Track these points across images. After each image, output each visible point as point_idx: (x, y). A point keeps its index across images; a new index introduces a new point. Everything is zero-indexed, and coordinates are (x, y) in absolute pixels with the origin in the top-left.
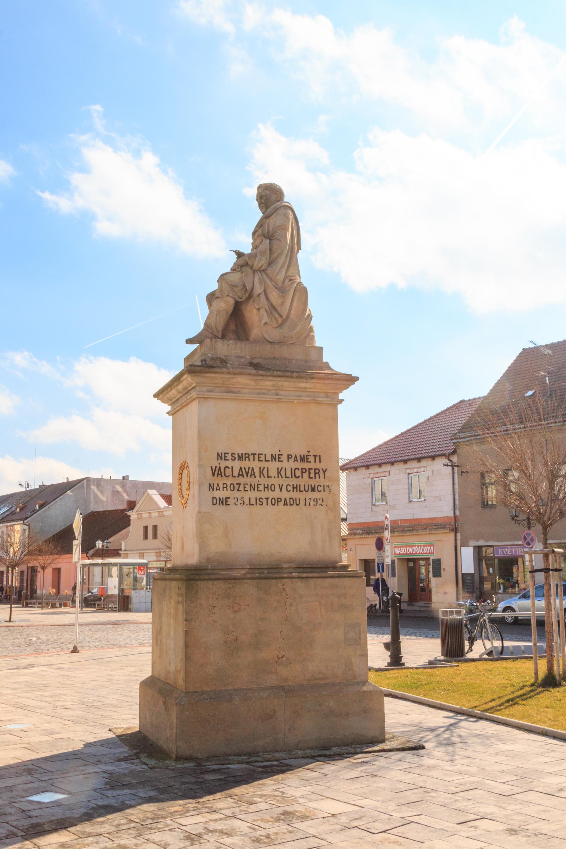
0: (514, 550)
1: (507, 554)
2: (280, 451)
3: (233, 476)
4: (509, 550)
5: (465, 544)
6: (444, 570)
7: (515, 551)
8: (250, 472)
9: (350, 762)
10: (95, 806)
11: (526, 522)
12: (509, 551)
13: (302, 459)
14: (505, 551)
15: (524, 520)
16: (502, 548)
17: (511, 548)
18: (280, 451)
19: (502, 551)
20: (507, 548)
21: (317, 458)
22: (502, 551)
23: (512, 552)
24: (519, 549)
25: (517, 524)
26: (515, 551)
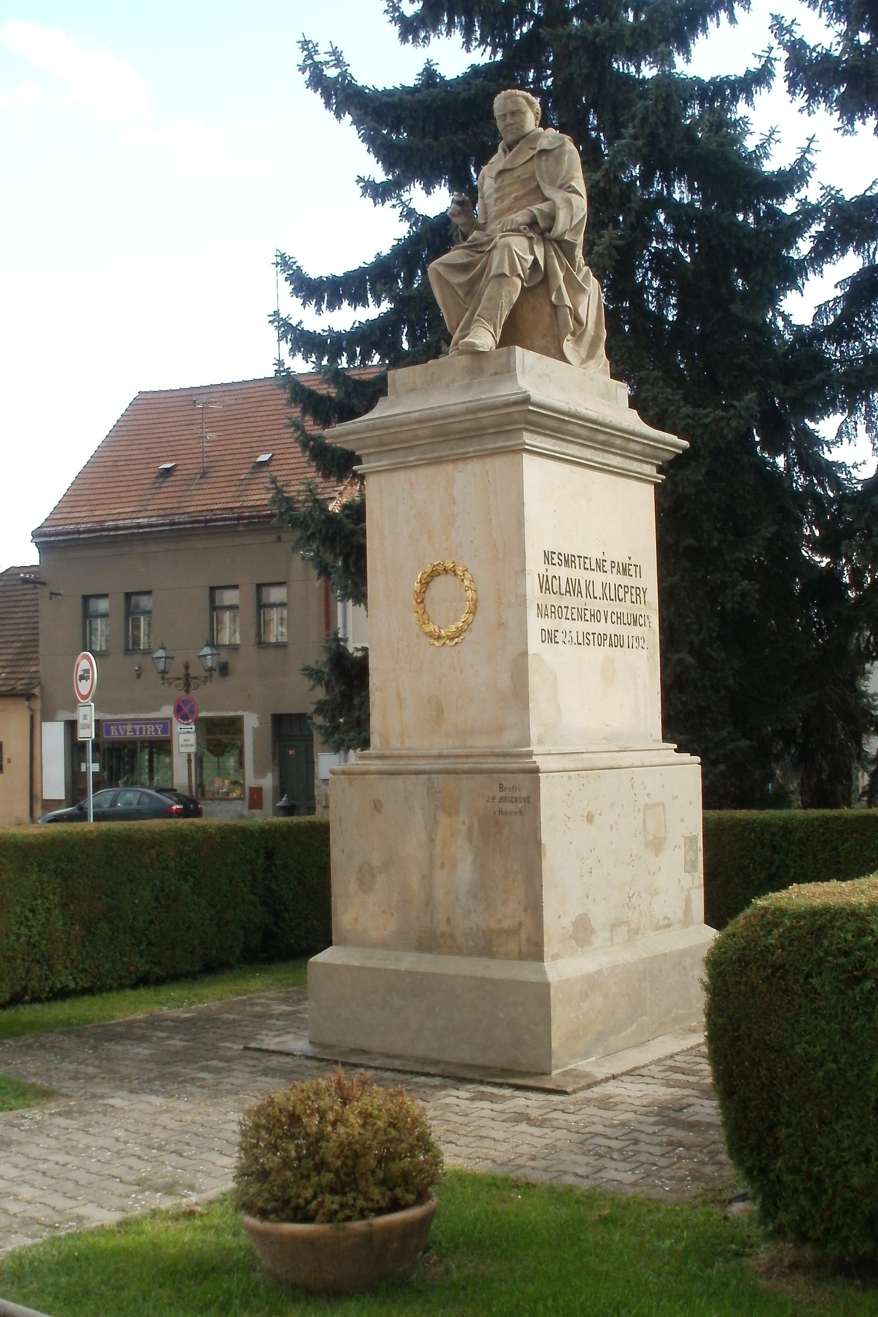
0: (137, 727)
1: (125, 734)
2: (630, 558)
3: (561, 594)
4: (129, 727)
5: (48, 716)
6: (9, 761)
7: (141, 731)
8: (573, 589)
9: (150, 1103)
10: (513, 1115)
11: (181, 682)
12: (129, 730)
13: (625, 570)
14: (123, 729)
15: (179, 679)
16: (117, 725)
17: (133, 724)
18: (630, 558)
19: (118, 730)
20: (126, 724)
21: (638, 568)
22: (118, 730)
23: (134, 730)
24: (148, 726)
25: (166, 685)
26: (141, 731)
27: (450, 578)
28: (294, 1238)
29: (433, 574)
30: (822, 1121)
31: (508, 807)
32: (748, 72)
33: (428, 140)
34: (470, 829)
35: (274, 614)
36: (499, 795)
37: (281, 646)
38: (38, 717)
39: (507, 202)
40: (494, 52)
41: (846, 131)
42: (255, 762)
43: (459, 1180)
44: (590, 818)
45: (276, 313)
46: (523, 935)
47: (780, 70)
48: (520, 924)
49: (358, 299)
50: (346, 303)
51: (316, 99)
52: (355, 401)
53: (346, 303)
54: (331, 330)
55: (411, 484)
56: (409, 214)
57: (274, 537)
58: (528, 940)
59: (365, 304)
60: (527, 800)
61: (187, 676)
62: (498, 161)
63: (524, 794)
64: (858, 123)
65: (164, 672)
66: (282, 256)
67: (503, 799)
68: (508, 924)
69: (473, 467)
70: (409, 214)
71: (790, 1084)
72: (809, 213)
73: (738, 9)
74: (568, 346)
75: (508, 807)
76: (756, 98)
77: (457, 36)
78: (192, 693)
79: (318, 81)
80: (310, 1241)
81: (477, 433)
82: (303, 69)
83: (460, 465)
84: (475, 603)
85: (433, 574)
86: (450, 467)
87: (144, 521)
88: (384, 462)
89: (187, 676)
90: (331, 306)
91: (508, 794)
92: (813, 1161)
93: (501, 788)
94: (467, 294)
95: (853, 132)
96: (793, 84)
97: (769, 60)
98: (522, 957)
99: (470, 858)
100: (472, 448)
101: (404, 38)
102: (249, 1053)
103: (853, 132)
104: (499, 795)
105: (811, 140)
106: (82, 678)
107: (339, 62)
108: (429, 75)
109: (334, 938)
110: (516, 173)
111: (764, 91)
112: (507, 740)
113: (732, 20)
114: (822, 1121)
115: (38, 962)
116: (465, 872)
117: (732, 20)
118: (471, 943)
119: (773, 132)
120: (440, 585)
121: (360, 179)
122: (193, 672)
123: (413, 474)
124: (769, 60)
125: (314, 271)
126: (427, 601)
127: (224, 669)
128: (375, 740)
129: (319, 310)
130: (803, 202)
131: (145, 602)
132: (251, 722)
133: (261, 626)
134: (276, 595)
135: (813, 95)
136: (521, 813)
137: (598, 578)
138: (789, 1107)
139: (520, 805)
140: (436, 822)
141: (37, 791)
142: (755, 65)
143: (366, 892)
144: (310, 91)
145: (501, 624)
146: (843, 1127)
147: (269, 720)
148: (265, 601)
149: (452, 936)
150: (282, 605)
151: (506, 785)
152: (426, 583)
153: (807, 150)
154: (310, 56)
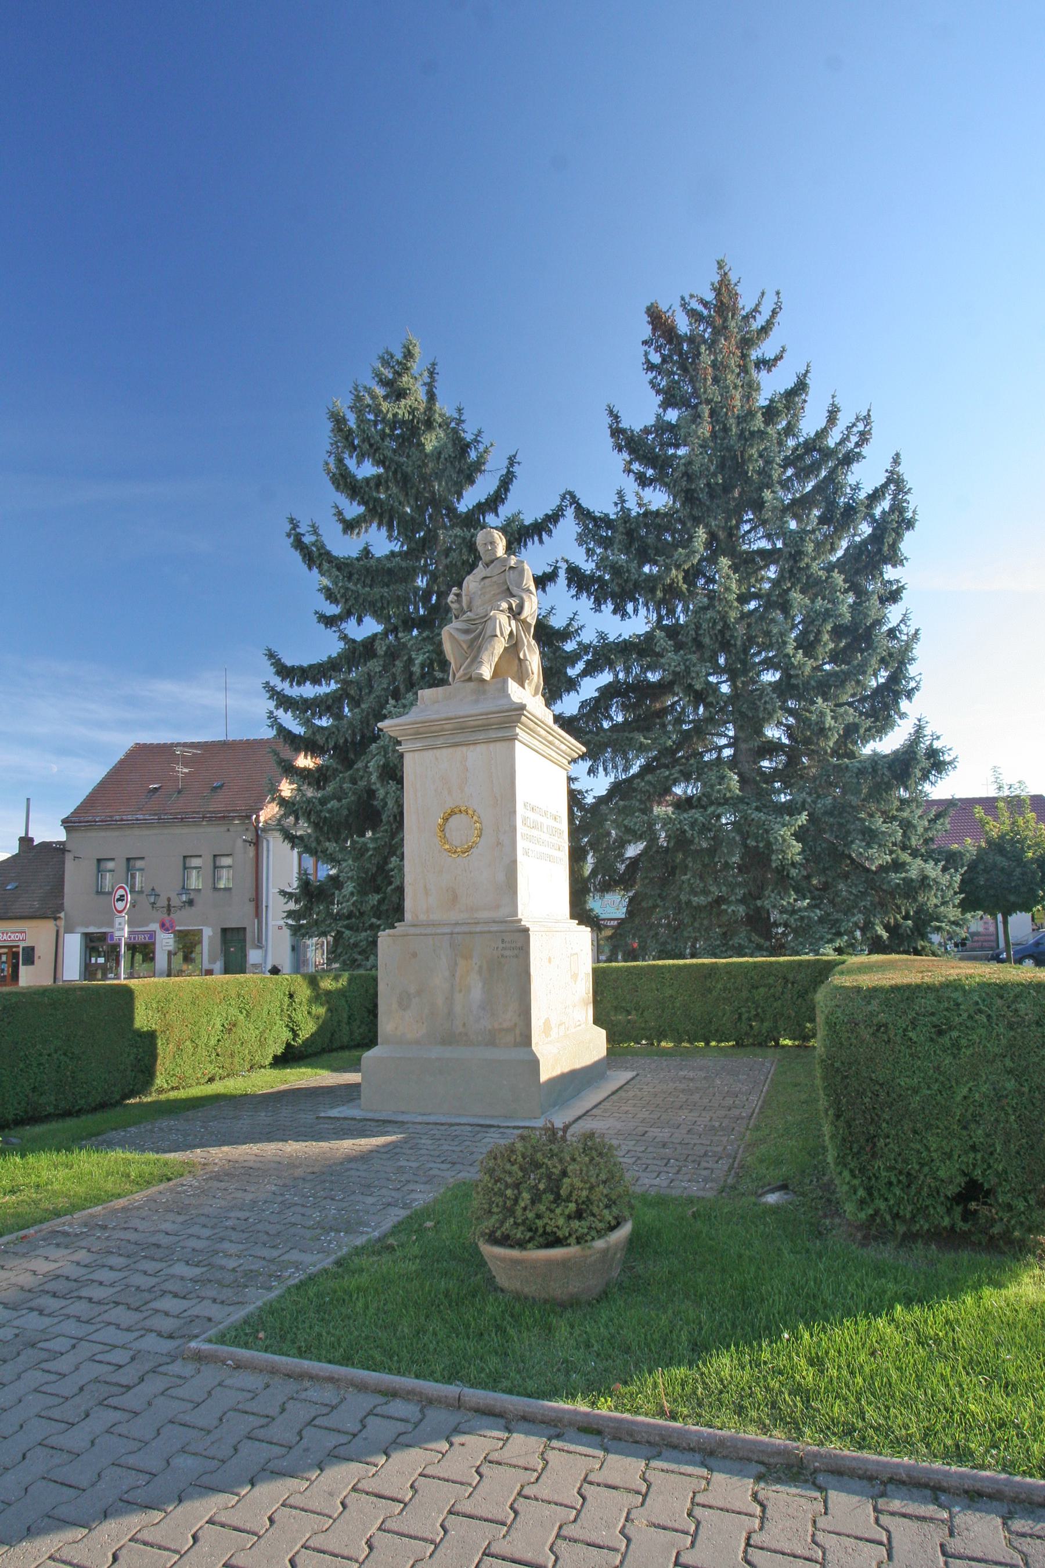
5: (69, 930)
27: (463, 816)
28: (549, 1262)
29: (452, 813)
30: (915, 1132)
31: (507, 953)
32: (544, 573)
33: (367, 589)
34: (480, 967)
35: (224, 873)
36: (501, 946)
37: (227, 889)
38: (62, 931)
39: (487, 596)
40: (402, 546)
41: (596, 611)
42: (209, 955)
43: (1006, 1236)
44: (550, 961)
45: (267, 683)
46: (517, 1031)
47: (562, 574)
48: (515, 1025)
49: (316, 682)
50: (308, 683)
51: (297, 556)
52: (318, 737)
53: (308, 683)
54: (301, 697)
55: (437, 759)
56: (344, 638)
57: (226, 829)
58: (521, 1034)
59: (320, 684)
60: (521, 948)
61: (169, 905)
62: (480, 571)
63: (519, 945)
64: (603, 607)
65: (154, 903)
66: (269, 650)
67: (504, 949)
68: (506, 1025)
69: (481, 748)
70: (344, 638)
71: (890, 1108)
72: (584, 648)
73: (544, 535)
74: (526, 686)
75: (507, 953)
76: (547, 589)
77: (384, 531)
78: (172, 915)
79: (299, 544)
80: (564, 1264)
81: (485, 727)
82: (289, 535)
83: (472, 748)
84: (481, 830)
85: (452, 813)
86: (464, 749)
87: (141, 817)
88: (418, 745)
89: (169, 905)
90: (299, 684)
91: (508, 945)
92: (906, 1161)
93: (503, 941)
94: (469, 647)
95: (600, 611)
96: (570, 581)
97: (556, 568)
98: (516, 1045)
99: (480, 985)
100: (481, 736)
101: (345, 531)
102: (321, 1120)
103: (600, 611)
104: (501, 946)
105: (575, 614)
106: (118, 900)
107: (315, 531)
108: (366, 552)
109: (379, 1040)
110: (494, 579)
111: (553, 585)
112: (502, 913)
113: (541, 541)
114: (915, 1132)
115: (142, 1071)
116: (477, 993)
117: (541, 541)
118: (480, 1038)
119: (552, 608)
120: (454, 821)
121: (316, 613)
122: (172, 903)
123: (438, 752)
124: (556, 568)
125: (289, 661)
126: (447, 830)
127: (191, 903)
128: (408, 916)
129: (291, 686)
130: (579, 644)
131: (139, 864)
132: (207, 932)
133: (215, 879)
134: (226, 861)
135: (580, 590)
136: (517, 956)
137: (543, 820)
138: (887, 1123)
139: (516, 952)
140: (456, 964)
141: (59, 975)
142: (549, 570)
143: (404, 1010)
144: (293, 550)
145: (499, 844)
146: (933, 1135)
147: (219, 930)
148: (218, 864)
149: (466, 1034)
150: (229, 867)
151: (506, 939)
152: (446, 820)
153: (572, 619)
154: (294, 529)
